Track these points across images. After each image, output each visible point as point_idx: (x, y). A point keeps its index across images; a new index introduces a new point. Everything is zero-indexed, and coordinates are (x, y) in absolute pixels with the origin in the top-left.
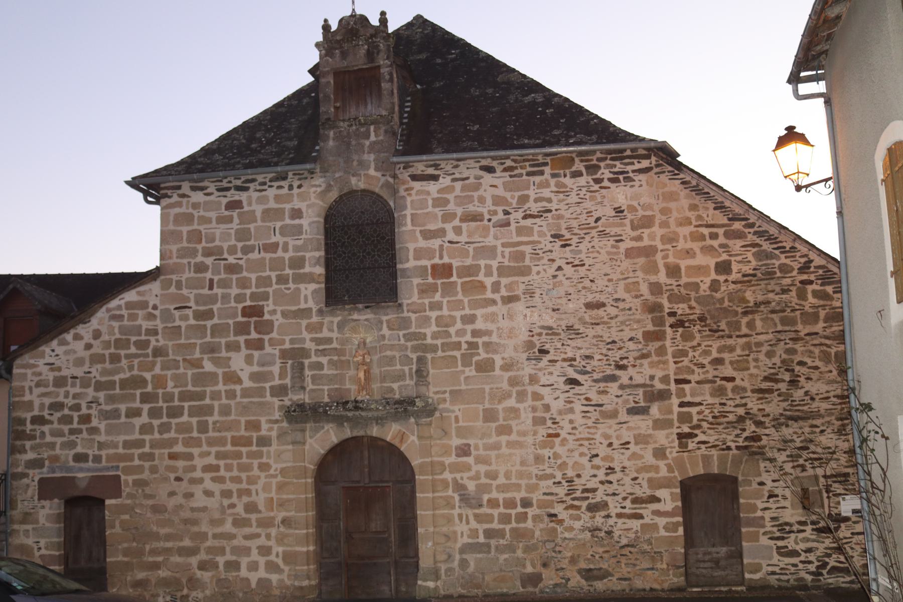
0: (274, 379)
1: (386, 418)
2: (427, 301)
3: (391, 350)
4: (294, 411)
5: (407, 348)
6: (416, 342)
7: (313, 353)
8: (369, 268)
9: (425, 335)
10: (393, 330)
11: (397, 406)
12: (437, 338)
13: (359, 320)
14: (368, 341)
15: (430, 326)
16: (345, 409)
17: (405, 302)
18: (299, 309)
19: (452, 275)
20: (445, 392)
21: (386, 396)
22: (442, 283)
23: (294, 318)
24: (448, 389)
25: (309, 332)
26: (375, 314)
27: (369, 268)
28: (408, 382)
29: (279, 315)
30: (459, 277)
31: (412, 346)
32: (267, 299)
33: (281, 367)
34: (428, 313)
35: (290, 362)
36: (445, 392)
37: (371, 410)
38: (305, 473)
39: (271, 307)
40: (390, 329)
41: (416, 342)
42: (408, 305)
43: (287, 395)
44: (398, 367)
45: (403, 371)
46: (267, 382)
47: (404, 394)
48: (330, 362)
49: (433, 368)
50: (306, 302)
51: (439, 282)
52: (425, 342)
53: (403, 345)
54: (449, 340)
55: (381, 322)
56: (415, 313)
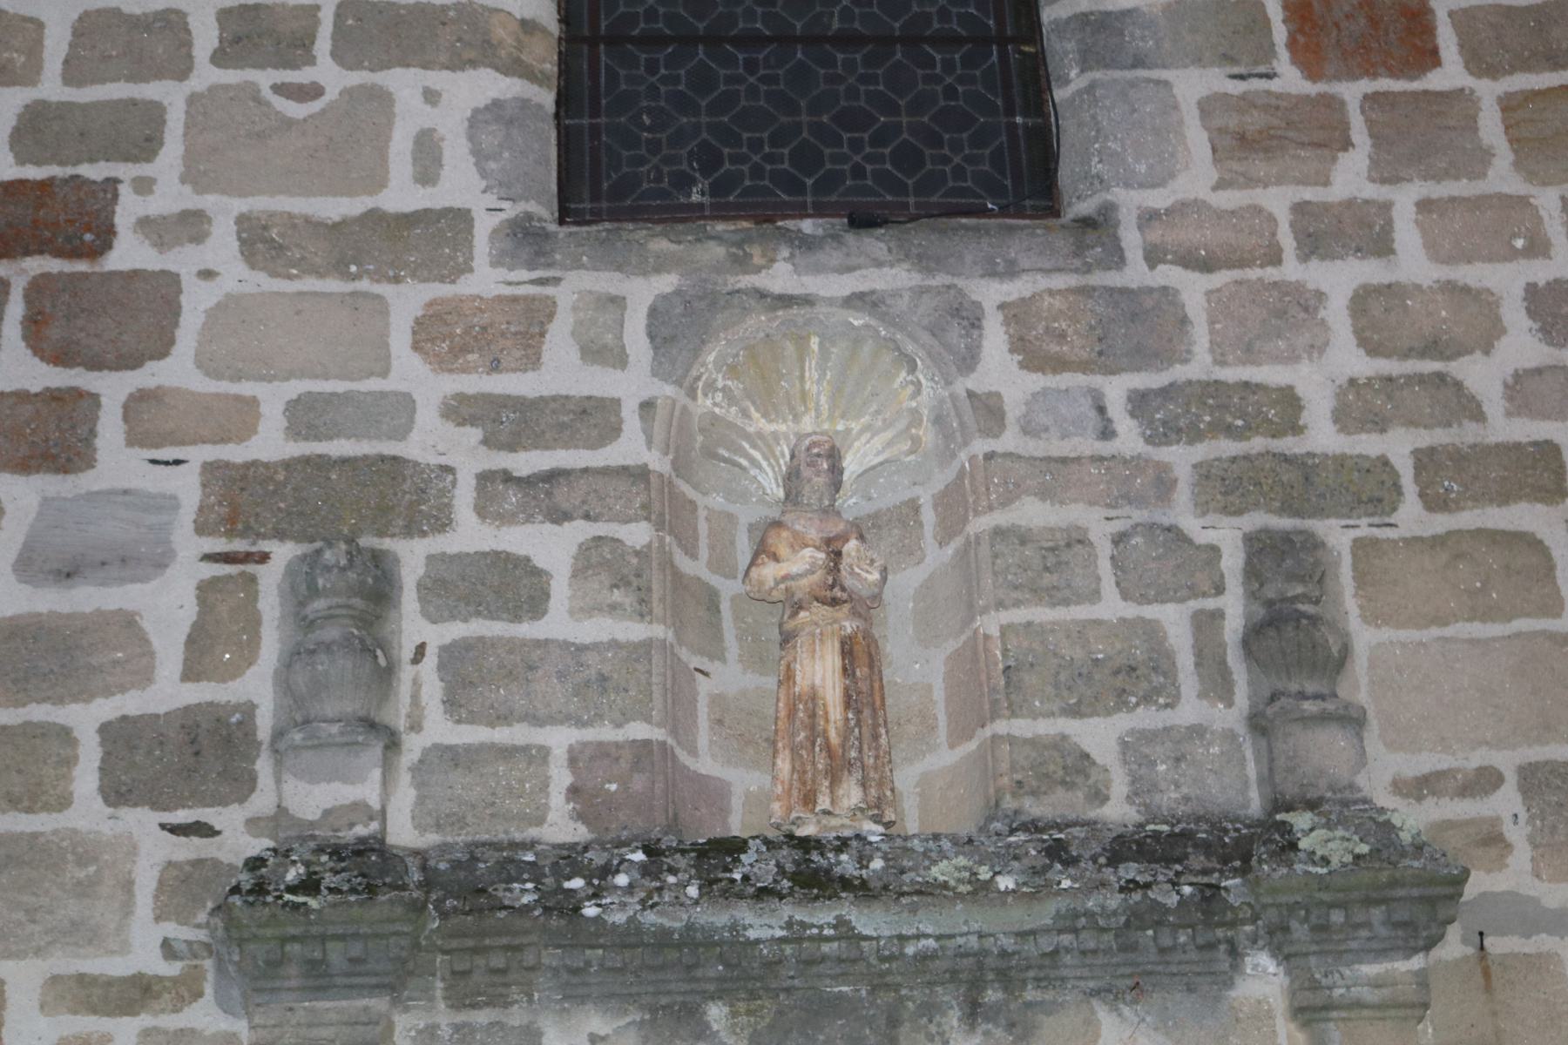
0: (145, 677)
1: (1048, 968)
2: (1278, 201)
3: (1044, 494)
4: (309, 885)
5: (1164, 484)
6: (1227, 447)
7: (464, 496)
8: (847, 40)
9: (1289, 400)
10: (1059, 365)
11: (1130, 870)
12: (1380, 424)
13: (807, 301)
14: (851, 465)
15: (1318, 349)
16: (716, 888)
17: (1129, 201)
18: (374, 217)
19: (1430, 58)
20: (1486, 781)
21: (1034, 808)
22: (1371, 100)
23: (339, 268)
24: (1507, 761)
25: (443, 365)
26: (925, 263)
27: (847, 40)
28: (1190, 710)
29: (222, 247)
30: (1478, 63)
31: (1204, 473)
32: (148, 147)
33: (206, 590)
34: (1291, 269)
35: (283, 552)
36: (1486, 781)
37: (930, 892)
38: (574, 972)
39: (170, 197)
40: (1033, 358)
41: (1227, 447)
42: (1149, 218)
43: (243, 786)
44: (1112, 607)
45: (1152, 632)
46: (84, 695)
47: (1168, 799)
48: (591, 559)
49: (1374, 618)
50: (427, 171)
51: (1352, 92)
52: (1289, 445)
53: (1136, 464)
54: (1466, 434)
55: (973, 321)
56: (1206, 266)
